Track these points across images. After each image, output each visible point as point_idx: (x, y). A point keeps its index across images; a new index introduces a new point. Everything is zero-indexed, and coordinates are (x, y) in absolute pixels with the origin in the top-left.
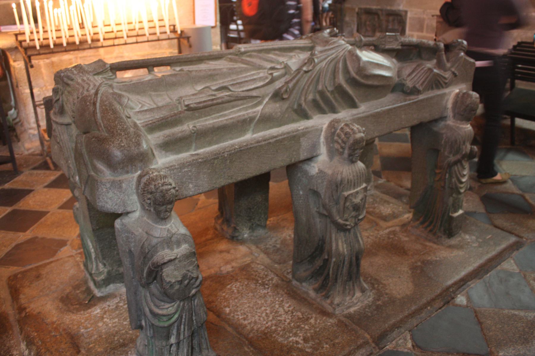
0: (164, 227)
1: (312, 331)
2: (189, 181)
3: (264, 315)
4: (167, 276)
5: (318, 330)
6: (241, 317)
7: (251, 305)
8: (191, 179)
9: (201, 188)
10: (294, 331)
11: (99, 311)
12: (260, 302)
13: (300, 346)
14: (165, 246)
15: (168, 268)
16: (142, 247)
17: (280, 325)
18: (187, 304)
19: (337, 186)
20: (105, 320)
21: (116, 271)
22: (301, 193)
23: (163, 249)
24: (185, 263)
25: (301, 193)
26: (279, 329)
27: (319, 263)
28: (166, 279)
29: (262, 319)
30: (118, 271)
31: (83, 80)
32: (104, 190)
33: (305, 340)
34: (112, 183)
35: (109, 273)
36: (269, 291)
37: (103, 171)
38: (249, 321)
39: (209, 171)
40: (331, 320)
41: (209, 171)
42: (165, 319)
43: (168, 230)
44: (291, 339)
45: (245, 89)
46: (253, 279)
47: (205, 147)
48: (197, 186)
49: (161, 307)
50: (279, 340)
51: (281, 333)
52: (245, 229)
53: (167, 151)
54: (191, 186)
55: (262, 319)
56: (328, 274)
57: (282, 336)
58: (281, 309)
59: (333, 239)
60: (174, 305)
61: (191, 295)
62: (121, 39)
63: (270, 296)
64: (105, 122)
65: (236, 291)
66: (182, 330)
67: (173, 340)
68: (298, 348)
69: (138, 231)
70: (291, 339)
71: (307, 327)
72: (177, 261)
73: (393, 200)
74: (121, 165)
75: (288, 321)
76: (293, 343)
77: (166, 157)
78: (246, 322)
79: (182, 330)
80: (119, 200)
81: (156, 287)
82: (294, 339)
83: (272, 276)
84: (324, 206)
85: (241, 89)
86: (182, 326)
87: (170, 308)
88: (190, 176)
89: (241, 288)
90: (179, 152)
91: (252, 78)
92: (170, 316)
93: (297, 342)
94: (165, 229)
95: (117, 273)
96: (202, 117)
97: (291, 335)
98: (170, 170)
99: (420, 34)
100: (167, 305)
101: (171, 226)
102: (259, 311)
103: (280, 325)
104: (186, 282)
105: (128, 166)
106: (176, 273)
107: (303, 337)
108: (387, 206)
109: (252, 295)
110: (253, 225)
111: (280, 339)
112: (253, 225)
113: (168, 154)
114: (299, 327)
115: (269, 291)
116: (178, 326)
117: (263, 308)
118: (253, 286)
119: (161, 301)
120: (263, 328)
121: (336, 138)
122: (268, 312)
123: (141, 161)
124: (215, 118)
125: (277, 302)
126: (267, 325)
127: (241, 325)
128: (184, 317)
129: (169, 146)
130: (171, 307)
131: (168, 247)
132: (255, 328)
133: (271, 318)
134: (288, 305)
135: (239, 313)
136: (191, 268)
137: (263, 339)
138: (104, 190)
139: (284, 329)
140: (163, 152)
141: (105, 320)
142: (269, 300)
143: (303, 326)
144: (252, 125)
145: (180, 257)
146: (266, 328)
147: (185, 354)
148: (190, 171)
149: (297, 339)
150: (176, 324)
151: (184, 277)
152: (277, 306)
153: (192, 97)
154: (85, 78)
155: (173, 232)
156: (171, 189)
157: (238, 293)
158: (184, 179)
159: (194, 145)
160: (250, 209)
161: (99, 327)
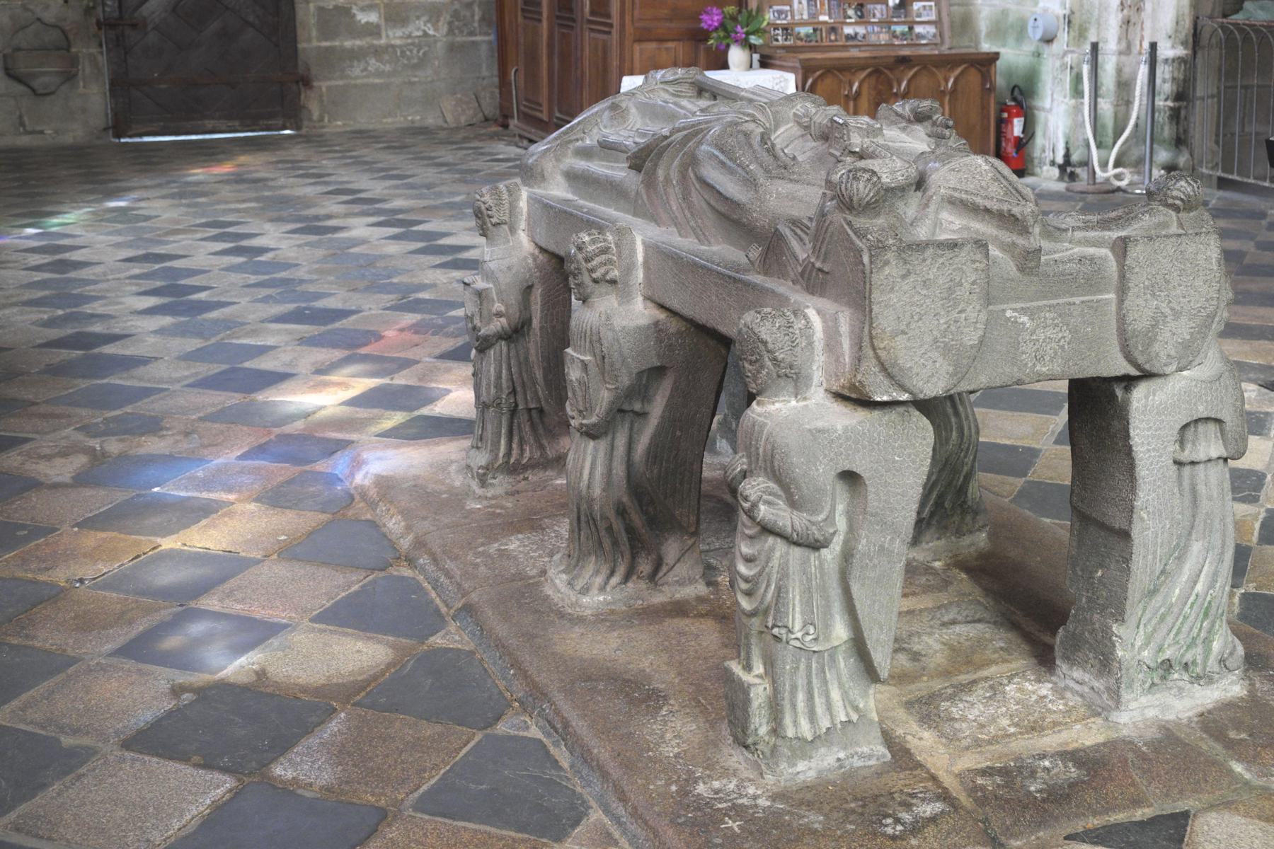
124: (607, 168)
129: (573, 177)
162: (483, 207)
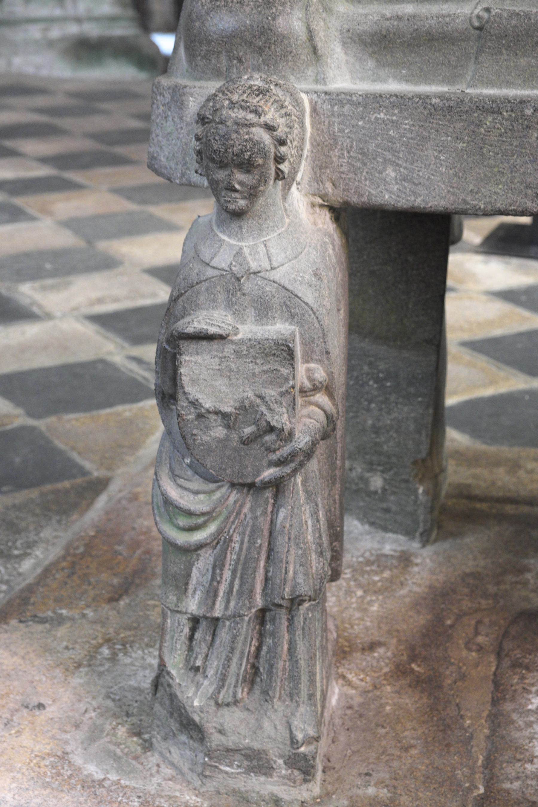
0: (233, 242)
2: (389, 156)
4: (194, 382)
14: (221, 297)
15: (199, 359)
18: (251, 509)
23: (213, 303)
28: (187, 389)
30: (366, 481)
34: (173, 89)
39: (461, 145)
41: (461, 145)
42: (182, 521)
43: (239, 253)
47: (509, 84)
48: (410, 181)
49: (181, 481)
53: (381, 64)
54: (391, 173)
60: (213, 491)
61: (258, 480)
72: (229, 349)
77: (377, 79)
88: (391, 139)
92: (195, 521)
94: (231, 246)
98: (330, 100)
101: (254, 251)
105: (219, 53)
106: (221, 384)
113: (383, 72)
123: (260, 50)
130: (204, 492)
131: (229, 305)
136: (271, 393)
140: (370, 64)
145: (241, 342)
148: (396, 125)
151: (245, 409)
155: (254, 266)
156: (252, 125)
158: (372, 147)
159: (472, 67)
162: (266, 138)
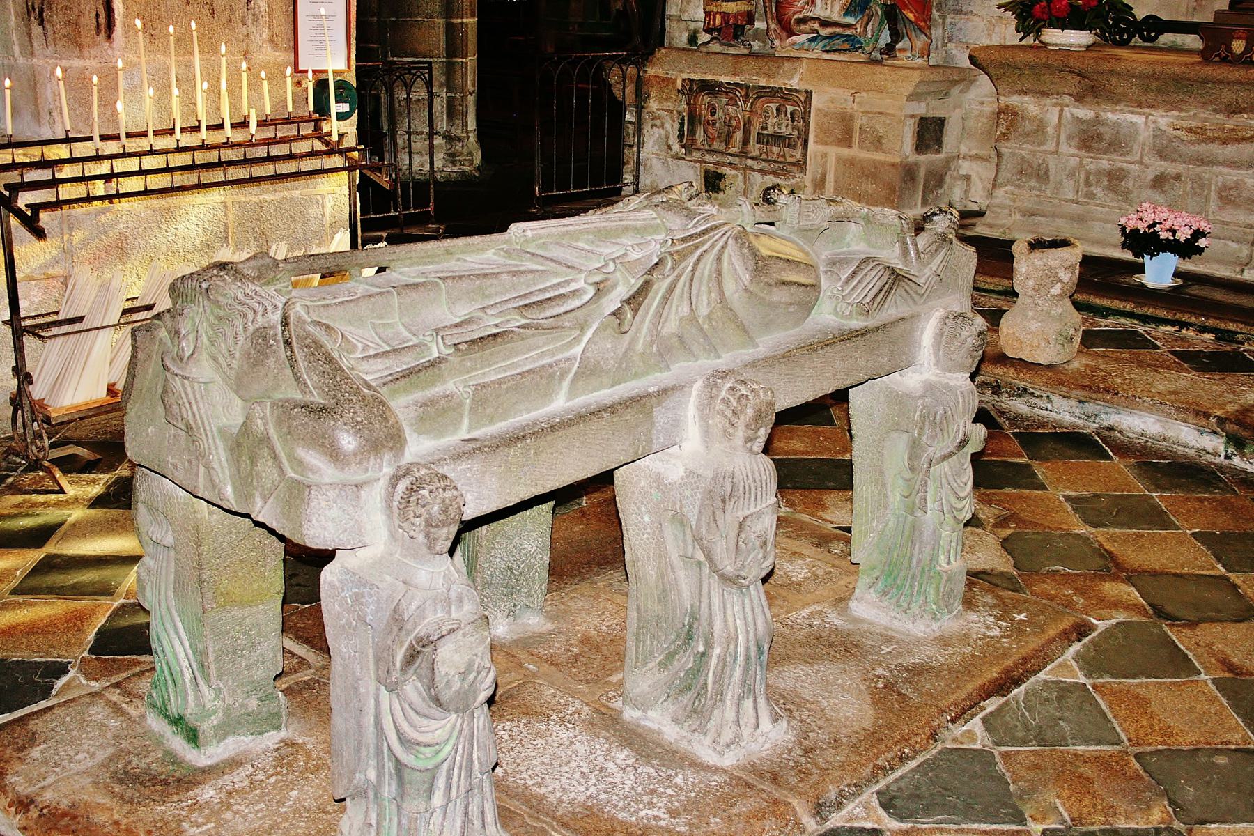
1: (682, 798)
3: (577, 775)
5: (693, 794)
6: (530, 783)
7: (546, 761)
8: (470, 485)
9: (486, 502)
10: (646, 799)
11: (212, 793)
12: (563, 754)
13: (663, 823)
16: (395, 611)
17: (616, 791)
19: (724, 501)
20: (235, 808)
21: (241, 706)
22: (647, 519)
24: (472, 639)
25: (647, 519)
26: (614, 797)
27: (686, 661)
29: (574, 782)
31: (246, 295)
32: (323, 504)
33: (672, 813)
35: (227, 711)
36: (577, 732)
37: (320, 469)
38: (550, 788)
40: (715, 778)
44: (642, 814)
45: (548, 314)
46: (537, 714)
50: (620, 817)
51: (621, 804)
52: (499, 616)
55: (574, 782)
56: (706, 684)
57: (623, 809)
58: (610, 765)
59: (716, 601)
62: (89, 144)
63: (582, 742)
64: (315, 378)
65: (506, 737)
66: (455, 778)
67: (438, 799)
68: (661, 827)
69: (384, 581)
70: (642, 814)
71: (669, 791)
73: (812, 551)
74: (358, 458)
75: (629, 783)
76: (649, 819)
78: (544, 790)
79: (455, 778)
80: (352, 523)
81: (416, 688)
82: (650, 812)
83: (578, 705)
84: (697, 539)
85: (542, 315)
86: (456, 771)
87: (439, 732)
89: (515, 730)
90: (441, 435)
91: (557, 293)
93: (656, 818)
95: (243, 711)
96: (477, 369)
97: (641, 806)
99: (845, 152)
100: (434, 724)
102: (565, 769)
103: (616, 791)
104: (471, 677)
106: (456, 657)
107: (667, 808)
108: (800, 562)
109: (543, 742)
110: (515, 606)
111: (621, 815)
112: (515, 606)
114: (652, 792)
115: (577, 732)
116: (448, 771)
117: (573, 765)
118: (540, 726)
119: (425, 716)
120: (582, 799)
121: (719, 407)
122: (583, 770)
125: (599, 752)
126: (589, 793)
127: (535, 796)
128: (460, 751)
132: (565, 798)
133: (593, 781)
134: (623, 756)
135: (524, 775)
137: (587, 816)
138: (323, 504)
139: (625, 798)
141: (235, 808)
142: (581, 749)
143: (662, 790)
144: (566, 384)
146: (588, 798)
147: (459, 830)
149: (656, 812)
150: (445, 766)
152: (601, 759)
153: (455, 331)
154: (248, 291)
157: (513, 740)
160: (511, 568)
161: (226, 821)
